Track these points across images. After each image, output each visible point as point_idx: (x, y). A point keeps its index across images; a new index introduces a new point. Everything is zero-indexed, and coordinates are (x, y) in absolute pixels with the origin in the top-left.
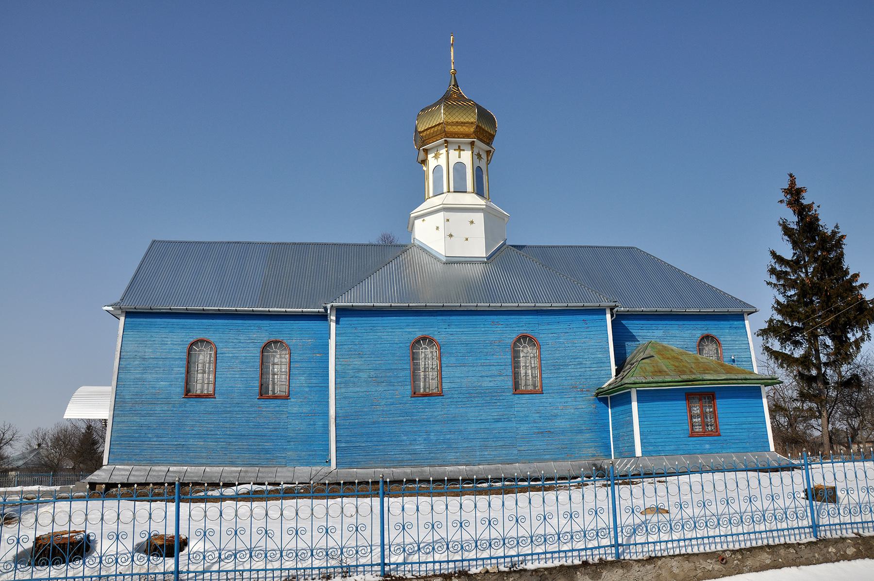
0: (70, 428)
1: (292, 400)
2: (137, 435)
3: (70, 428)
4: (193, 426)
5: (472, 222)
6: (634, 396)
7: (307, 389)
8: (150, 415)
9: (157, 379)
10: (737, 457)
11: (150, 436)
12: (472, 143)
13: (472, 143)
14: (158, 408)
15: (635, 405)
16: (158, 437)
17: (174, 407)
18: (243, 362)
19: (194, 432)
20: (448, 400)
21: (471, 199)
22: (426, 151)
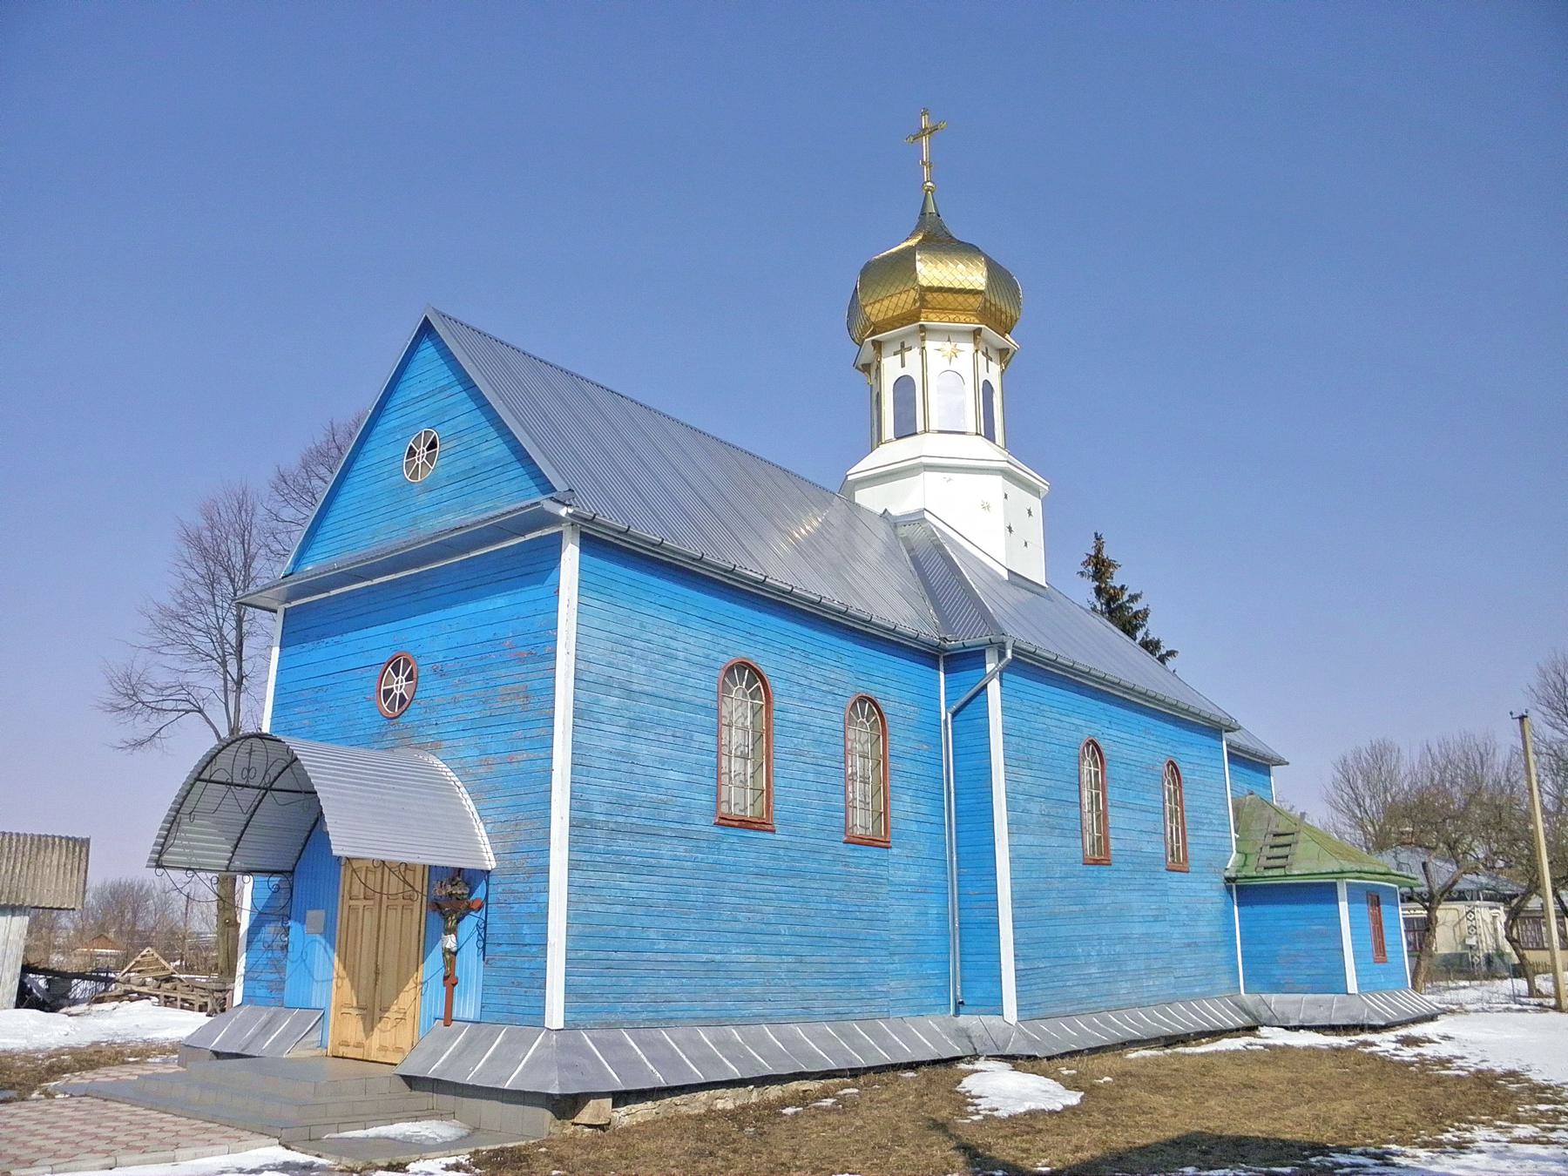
0: (1501, 758)
1: (894, 851)
2: (623, 933)
3: (1501, 758)
4: (736, 908)
5: (986, 507)
6: (1342, 892)
7: (914, 827)
8: (651, 870)
9: (662, 760)
10: (741, 1033)
11: (652, 934)
12: (976, 333)
13: (976, 333)
14: (665, 851)
15: (1343, 906)
16: (668, 938)
17: (699, 850)
18: (818, 742)
19: (738, 926)
20: (1116, 874)
21: (992, 453)
22: (878, 345)
